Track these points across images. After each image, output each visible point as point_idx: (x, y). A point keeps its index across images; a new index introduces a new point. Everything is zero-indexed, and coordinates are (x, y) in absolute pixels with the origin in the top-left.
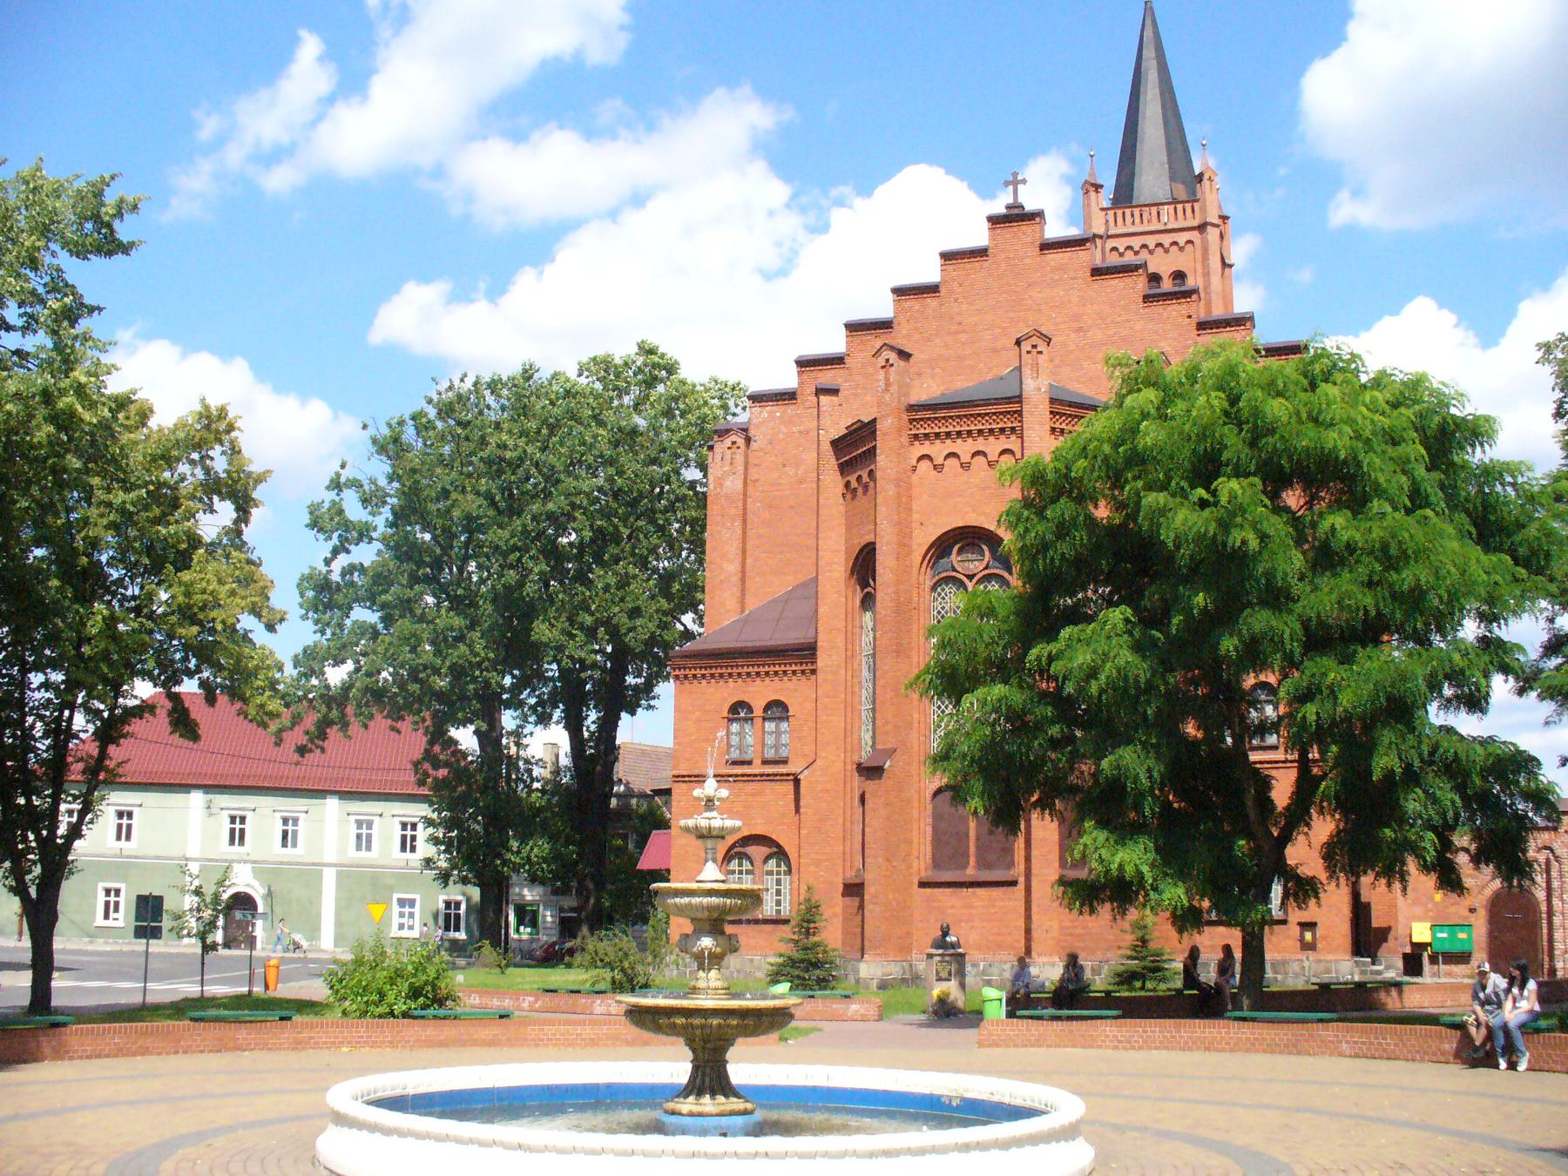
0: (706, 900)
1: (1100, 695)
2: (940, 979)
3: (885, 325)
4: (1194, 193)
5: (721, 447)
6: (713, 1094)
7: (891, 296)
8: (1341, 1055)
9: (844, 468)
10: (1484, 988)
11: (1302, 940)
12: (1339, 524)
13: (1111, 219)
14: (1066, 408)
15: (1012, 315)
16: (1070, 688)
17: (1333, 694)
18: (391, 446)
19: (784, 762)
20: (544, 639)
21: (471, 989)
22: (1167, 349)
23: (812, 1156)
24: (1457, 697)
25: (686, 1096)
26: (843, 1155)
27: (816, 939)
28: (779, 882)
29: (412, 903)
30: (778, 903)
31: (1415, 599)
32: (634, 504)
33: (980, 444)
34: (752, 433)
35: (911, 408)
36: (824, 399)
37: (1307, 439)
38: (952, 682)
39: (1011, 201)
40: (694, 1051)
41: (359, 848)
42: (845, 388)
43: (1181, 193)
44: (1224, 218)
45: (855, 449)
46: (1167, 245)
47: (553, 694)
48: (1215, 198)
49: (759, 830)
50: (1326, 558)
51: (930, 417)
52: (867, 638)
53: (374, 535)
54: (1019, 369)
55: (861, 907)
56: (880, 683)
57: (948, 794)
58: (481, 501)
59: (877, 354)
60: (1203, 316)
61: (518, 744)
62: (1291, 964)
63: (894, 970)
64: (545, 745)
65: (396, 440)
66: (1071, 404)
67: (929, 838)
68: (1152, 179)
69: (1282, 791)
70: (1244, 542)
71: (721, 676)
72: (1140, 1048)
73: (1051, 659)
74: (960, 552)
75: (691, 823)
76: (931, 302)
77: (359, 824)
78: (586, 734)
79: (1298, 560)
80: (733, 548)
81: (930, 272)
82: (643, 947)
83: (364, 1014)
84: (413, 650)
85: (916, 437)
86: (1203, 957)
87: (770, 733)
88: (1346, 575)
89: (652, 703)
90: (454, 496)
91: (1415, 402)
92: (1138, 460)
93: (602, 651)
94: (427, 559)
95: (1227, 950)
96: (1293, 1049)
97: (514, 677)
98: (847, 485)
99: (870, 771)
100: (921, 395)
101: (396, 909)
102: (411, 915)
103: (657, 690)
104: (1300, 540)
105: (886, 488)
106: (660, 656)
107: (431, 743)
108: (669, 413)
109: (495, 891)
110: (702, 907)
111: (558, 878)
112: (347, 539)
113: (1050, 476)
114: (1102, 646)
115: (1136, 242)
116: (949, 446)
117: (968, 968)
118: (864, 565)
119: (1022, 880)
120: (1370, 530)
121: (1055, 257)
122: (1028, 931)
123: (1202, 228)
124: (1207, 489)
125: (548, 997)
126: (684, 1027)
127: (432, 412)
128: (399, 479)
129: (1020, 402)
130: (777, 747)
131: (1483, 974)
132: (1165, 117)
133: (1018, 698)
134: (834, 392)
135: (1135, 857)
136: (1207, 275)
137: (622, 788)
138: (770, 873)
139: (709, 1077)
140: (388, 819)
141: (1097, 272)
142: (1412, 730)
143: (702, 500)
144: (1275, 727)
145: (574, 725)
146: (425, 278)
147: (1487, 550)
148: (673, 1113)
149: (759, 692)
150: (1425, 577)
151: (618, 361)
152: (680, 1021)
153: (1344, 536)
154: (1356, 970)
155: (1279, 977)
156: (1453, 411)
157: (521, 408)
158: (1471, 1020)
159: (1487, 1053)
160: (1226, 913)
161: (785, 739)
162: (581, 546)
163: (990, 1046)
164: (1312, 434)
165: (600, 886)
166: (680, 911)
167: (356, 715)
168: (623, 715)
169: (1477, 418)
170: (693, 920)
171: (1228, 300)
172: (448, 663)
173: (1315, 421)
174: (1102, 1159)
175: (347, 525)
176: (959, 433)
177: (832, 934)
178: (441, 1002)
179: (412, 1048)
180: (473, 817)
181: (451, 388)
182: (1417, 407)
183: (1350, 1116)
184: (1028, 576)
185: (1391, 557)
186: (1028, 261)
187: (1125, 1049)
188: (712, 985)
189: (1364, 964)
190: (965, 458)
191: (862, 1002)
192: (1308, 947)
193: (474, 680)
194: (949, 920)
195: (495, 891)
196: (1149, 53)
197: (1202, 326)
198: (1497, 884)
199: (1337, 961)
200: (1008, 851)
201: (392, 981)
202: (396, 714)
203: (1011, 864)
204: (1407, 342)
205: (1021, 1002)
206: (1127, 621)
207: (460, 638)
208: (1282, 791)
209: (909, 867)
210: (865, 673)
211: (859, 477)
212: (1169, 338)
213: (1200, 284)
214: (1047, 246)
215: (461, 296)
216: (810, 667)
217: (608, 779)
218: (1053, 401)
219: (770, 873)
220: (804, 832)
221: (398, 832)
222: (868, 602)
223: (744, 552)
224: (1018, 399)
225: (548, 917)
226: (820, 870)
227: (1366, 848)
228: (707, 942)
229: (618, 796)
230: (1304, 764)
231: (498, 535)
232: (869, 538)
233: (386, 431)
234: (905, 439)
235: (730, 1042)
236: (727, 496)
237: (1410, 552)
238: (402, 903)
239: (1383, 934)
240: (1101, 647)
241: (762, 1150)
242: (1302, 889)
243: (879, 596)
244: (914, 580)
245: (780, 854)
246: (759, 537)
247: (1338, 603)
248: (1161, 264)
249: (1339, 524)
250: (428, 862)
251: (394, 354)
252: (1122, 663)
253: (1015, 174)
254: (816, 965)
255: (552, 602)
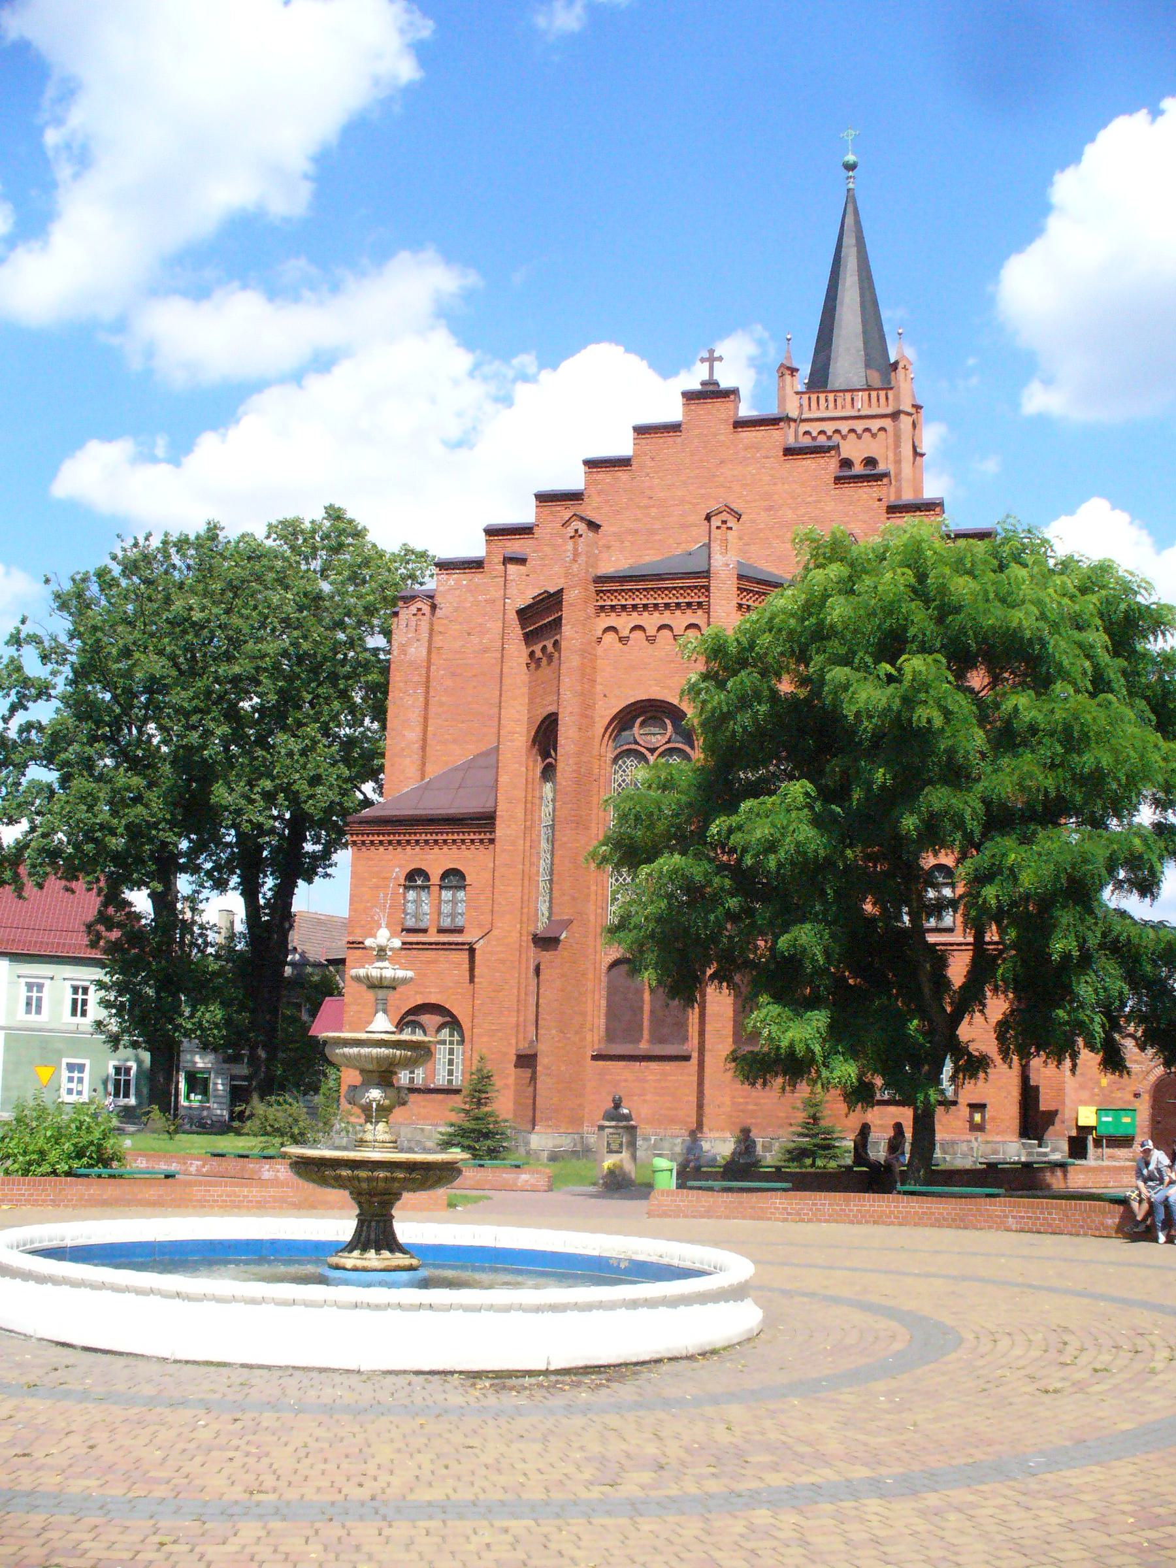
0: (375, 1051)
1: (779, 869)
2: (610, 1151)
3: (575, 497)
4: (889, 382)
5: (407, 613)
6: (378, 1250)
7: (582, 468)
8: (1009, 1230)
9: (529, 638)
10: (1147, 1164)
11: (971, 1120)
12: (1022, 704)
13: (805, 402)
14: (754, 585)
15: (703, 491)
16: (749, 861)
17: (1013, 876)
18: (73, 602)
19: (460, 931)
20: (224, 803)
21: (141, 1153)
22: (856, 531)
23: (478, 1309)
24: (1129, 880)
25: (351, 1251)
26: (508, 1309)
27: (486, 1109)
28: (451, 1052)
29: (81, 1068)
30: (450, 1073)
31: (1094, 781)
32: (315, 670)
33: (667, 617)
34: (438, 600)
35: (599, 580)
36: (512, 568)
37: (993, 617)
38: (630, 853)
39: (706, 377)
40: (360, 1204)
41: (28, 1012)
42: (533, 556)
43: (876, 379)
44: (917, 407)
45: (541, 619)
46: (859, 431)
47: (229, 861)
48: (908, 387)
49: (433, 1000)
50: (1008, 738)
51: (614, 588)
52: (546, 810)
53: (53, 692)
54: (708, 546)
55: (533, 1079)
56: (558, 853)
57: (625, 968)
58: (164, 661)
59: (565, 525)
60: (892, 499)
61: (193, 910)
62: (957, 1144)
63: (565, 1142)
64: (221, 911)
65: (79, 595)
66: (760, 582)
67: (603, 1010)
68: (848, 365)
69: (958, 970)
70: (929, 721)
71: (399, 842)
72: (810, 1221)
73: (730, 831)
74: (642, 724)
75: (362, 972)
76: (623, 475)
77: (30, 987)
78: (262, 902)
79: (979, 738)
80: (415, 716)
81: (624, 446)
82: (313, 1112)
83: (26, 1173)
84: (90, 808)
85: (602, 608)
86: (873, 1137)
87: (447, 902)
88: (1029, 756)
89: (329, 871)
90: (137, 655)
91: (1103, 587)
92: (822, 634)
93: (280, 817)
94: (107, 719)
95: (898, 1127)
96: (961, 1223)
97: (190, 841)
98: (532, 654)
99: (546, 942)
100: (608, 567)
101: (65, 1074)
102: (80, 1080)
103: (335, 857)
104: (982, 720)
105: (570, 658)
106: (341, 823)
107: (106, 905)
108: (354, 578)
109: (166, 1057)
110: (369, 1058)
111: (229, 1046)
112: (25, 696)
113: (733, 649)
114: (781, 819)
115: (829, 427)
116: (635, 619)
117: (639, 1143)
118: (545, 736)
119: (695, 1055)
120: (1052, 711)
121: (749, 436)
122: (700, 1106)
123: (895, 415)
124: (893, 665)
125: (216, 1161)
126: (350, 1179)
127: (116, 570)
128: (80, 636)
129: (708, 577)
130: (453, 915)
131: (1147, 1152)
132: (862, 304)
133: (697, 870)
134: (522, 561)
135: (805, 1030)
136: (898, 462)
137: (297, 957)
138: (443, 1042)
139: (375, 1233)
140: (60, 983)
141: (789, 452)
142: (1091, 912)
143: (385, 670)
144: (953, 904)
145: (250, 892)
146: (108, 436)
147: (1166, 738)
148: (337, 1267)
149: (436, 861)
150: (1106, 760)
151: (307, 525)
152: (345, 1173)
153: (1027, 716)
154: (1023, 1152)
155: (948, 1158)
156: (1139, 599)
157: (206, 571)
158: (1134, 1195)
159: (1147, 1227)
160: (899, 1090)
161: (461, 908)
162: (261, 709)
163: (660, 1216)
164: (999, 613)
165: (272, 1049)
166: (350, 1061)
167: (30, 875)
168: (300, 882)
169: (1161, 607)
170: (362, 1071)
171: (918, 487)
172: (123, 822)
173: (1003, 601)
174: (770, 1321)
175: (26, 682)
176: (645, 606)
177: (503, 1104)
178: (105, 1162)
179: (74, 1207)
180: (145, 982)
181: (136, 545)
182: (1103, 592)
183: (1017, 1285)
184: (710, 749)
185: (1073, 738)
186: (722, 438)
187: (793, 1221)
188: (380, 1138)
189: (1031, 1146)
190: (651, 631)
191: (532, 1172)
192: (977, 1125)
193: (151, 840)
194: (621, 1093)
195: (166, 1057)
196: (849, 241)
197: (892, 509)
198: (1160, 1071)
199: (1004, 1142)
200: (682, 1025)
201: (57, 1140)
202: (71, 874)
203: (685, 1039)
204: (1091, 534)
205: (692, 1173)
206: (807, 794)
207: (138, 799)
208: (958, 970)
209: (583, 1039)
210: (544, 845)
211: (544, 648)
212: (860, 519)
213: (892, 469)
214: (741, 424)
215: (147, 457)
216: (488, 836)
217: (283, 947)
218: (740, 577)
219: (443, 1042)
220: (477, 1002)
221: (69, 996)
222: (548, 773)
223: (426, 719)
224: (706, 574)
225: (219, 1085)
226: (494, 1038)
227: (1038, 1030)
228: (375, 1094)
229: (293, 964)
230: (979, 945)
231: (179, 697)
232: (552, 709)
233: (67, 586)
234: (591, 610)
235: (397, 1196)
236: (411, 663)
237: (1091, 734)
238: (71, 1067)
239: (1050, 1117)
240: (781, 819)
241: (426, 1301)
242: (973, 1066)
243: (560, 766)
244: (595, 752)
245: (453, 1023)
246: (442, 704)
247: (1020, 784)
248: (855, 450)
249: (1022, 704)
250: (99, 1024)
251: (76, 513)
252: (801, 838)
253: (712, 351)
254: (487, 1136)
255: (232, 766)
